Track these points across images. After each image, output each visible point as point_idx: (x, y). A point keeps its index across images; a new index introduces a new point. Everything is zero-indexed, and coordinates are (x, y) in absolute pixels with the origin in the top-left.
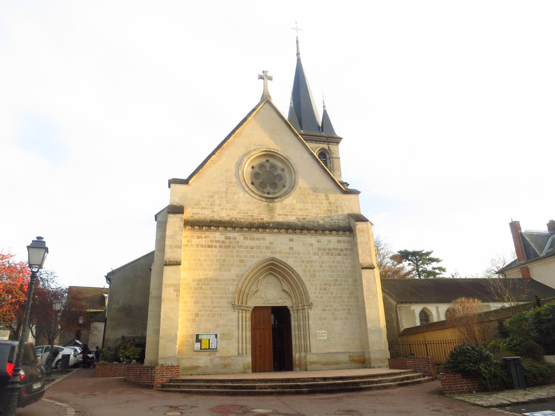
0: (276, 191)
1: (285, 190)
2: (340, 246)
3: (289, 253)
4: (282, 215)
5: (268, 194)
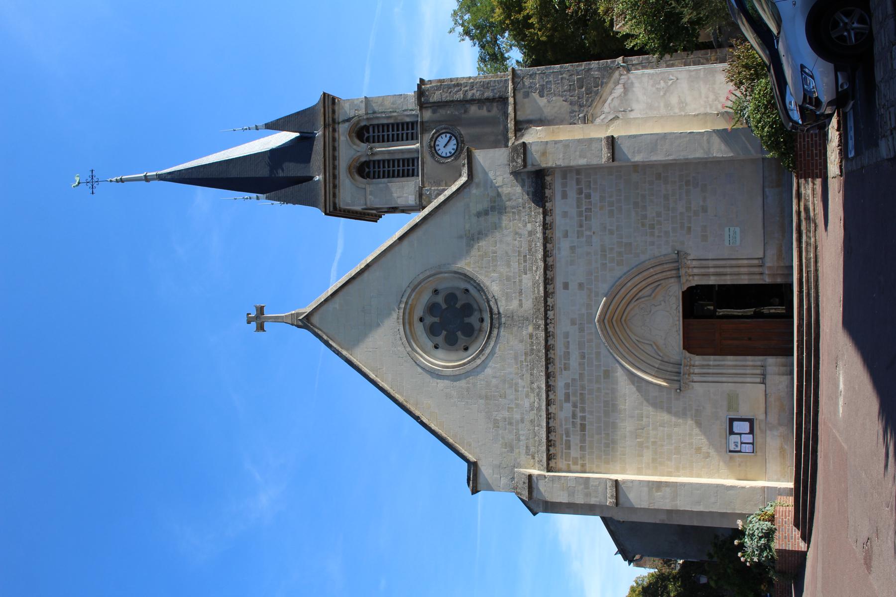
0: (475, 306)
1: (472, 291)
2: (572, 194)
4: (520, 300)
5: (482, 320)
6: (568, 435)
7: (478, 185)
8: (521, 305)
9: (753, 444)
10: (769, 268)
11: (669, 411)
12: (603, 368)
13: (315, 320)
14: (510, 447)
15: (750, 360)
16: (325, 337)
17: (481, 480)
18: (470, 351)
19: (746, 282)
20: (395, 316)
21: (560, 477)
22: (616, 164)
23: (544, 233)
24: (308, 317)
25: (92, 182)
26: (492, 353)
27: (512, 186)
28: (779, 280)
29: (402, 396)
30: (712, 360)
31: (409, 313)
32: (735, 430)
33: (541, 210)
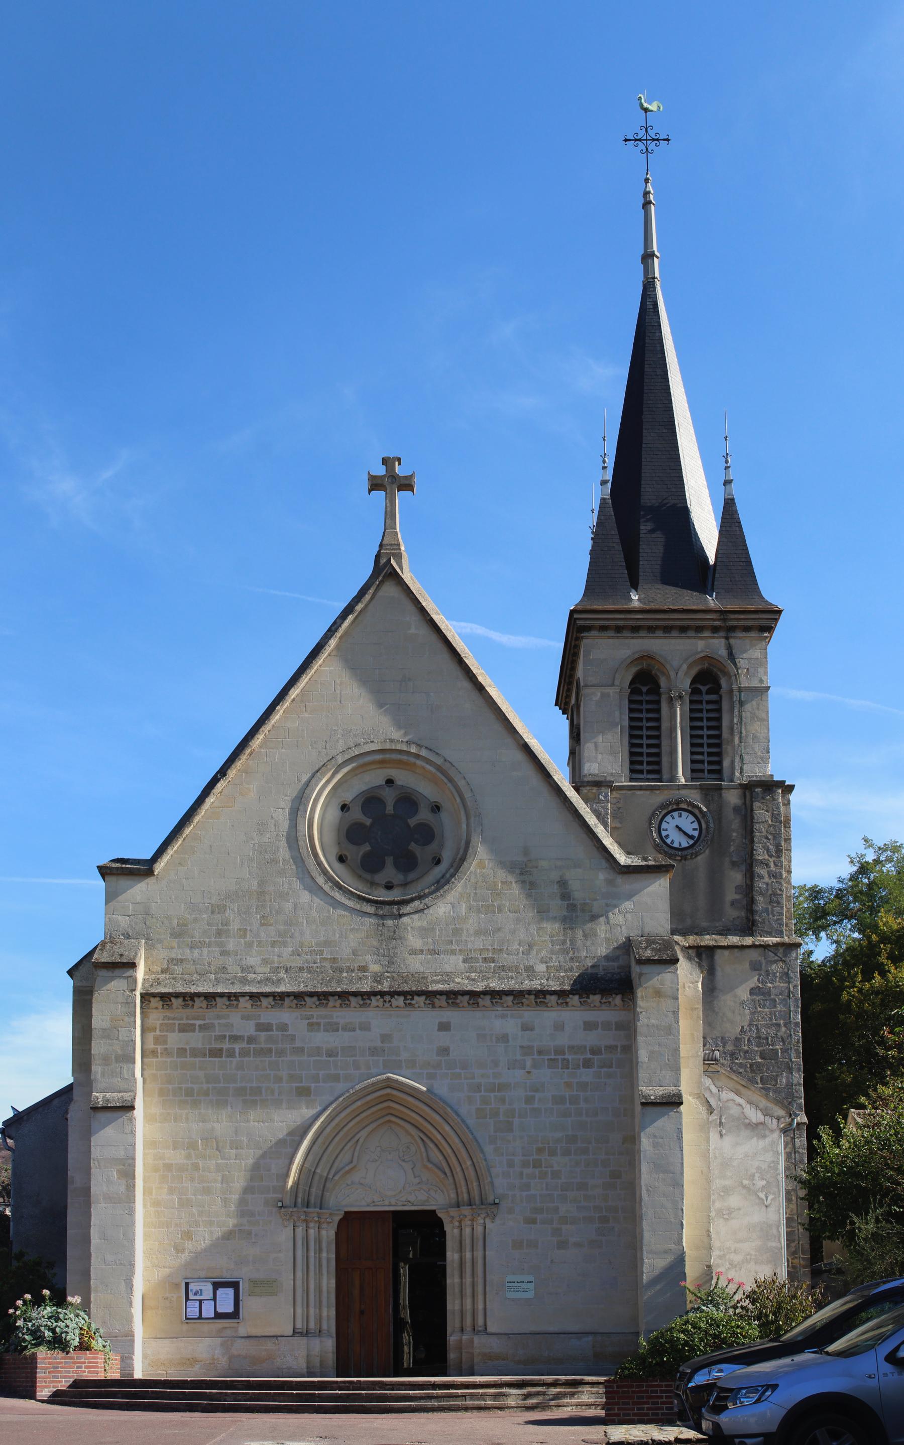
0: (411, 876)
1: (438, 871)
2: (592, 1039)
4: (421, 951)
5: (389, 887)
7: (610, 882)
8: (413, 952)
9: (200, 1318)
11: (247, 1190)
15: (329, 1313)
16: (359, 607)
17: (123, 882)
18: (337, 865)
19: (449, 1307)
20: (397, 735)
21: (134, 1014)
23: (529, 992)
24: (395, 577)
25: (647, 140)
27: (607, 939)
28: (452, 1356)
29: (260, 747)
30: (329, 1255)
32: (220, 1292)
33: (567, 987)
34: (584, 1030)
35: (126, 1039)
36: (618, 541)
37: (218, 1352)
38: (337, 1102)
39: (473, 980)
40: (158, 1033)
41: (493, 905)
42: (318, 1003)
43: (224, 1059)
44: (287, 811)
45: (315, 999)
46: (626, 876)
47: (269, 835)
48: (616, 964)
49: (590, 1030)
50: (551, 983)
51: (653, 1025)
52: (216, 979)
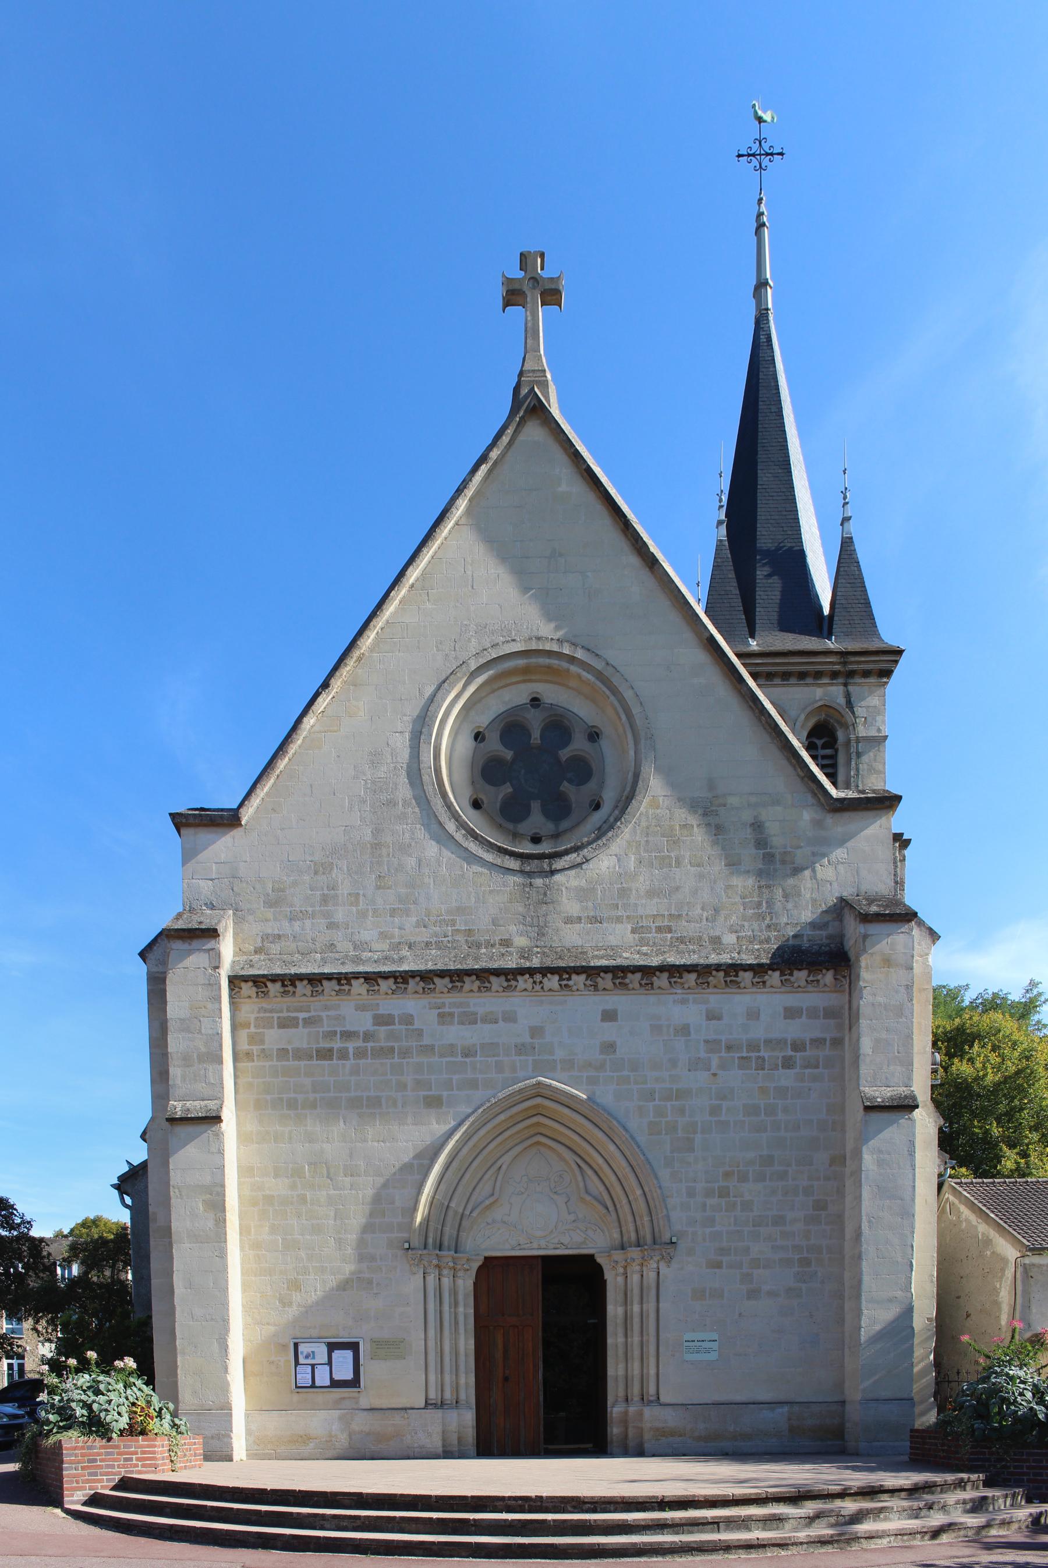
0: (565, 825)
1: (597, 817)
2: (794, 1030)
3: (601, 1067)
4: (579, 919)
5: (536, 840)
6: (308, 1022)
7: (818, 824)
8: (569, 920)
9: (313, 1386)
10: (640, 1414)
11: (368, 1228)
12: (445, 1094)
13: (534, 432)
14: (275, 901)
15: (468, 1380)
16: (494, 454)
17: (203, 835)
18: (472, 812)
19: (611, 1371)
20: (546, 629)
21: (218, 999)
22: (855, 1113)
23: (718, 967)
24: (538, 410)
25: (760, 154)
26: (472, 859)
27: (814, 901)
28: (614, 1431)
29: (372, 649)
30: (466, 1311)
31: (549, 667)
32: (337, 1354)
33: (765, 961)
34: (785, 1018)
35: (210, 1032)
36: (735, 584)
37: (336, 1427)
38: (476, 1115)
39: (646, 954)
40: (253, 1029)
41: (669, 857)
42: (450, 986)
43: (335, 1061)
44: (407, 735)
45: (447, 980)
46: (838, 815)
47: (384, 768)
48: (824, 933)
49: (793, 1018)
50: (744, 956)
51: (880, 1004)
52: (322, 959)
